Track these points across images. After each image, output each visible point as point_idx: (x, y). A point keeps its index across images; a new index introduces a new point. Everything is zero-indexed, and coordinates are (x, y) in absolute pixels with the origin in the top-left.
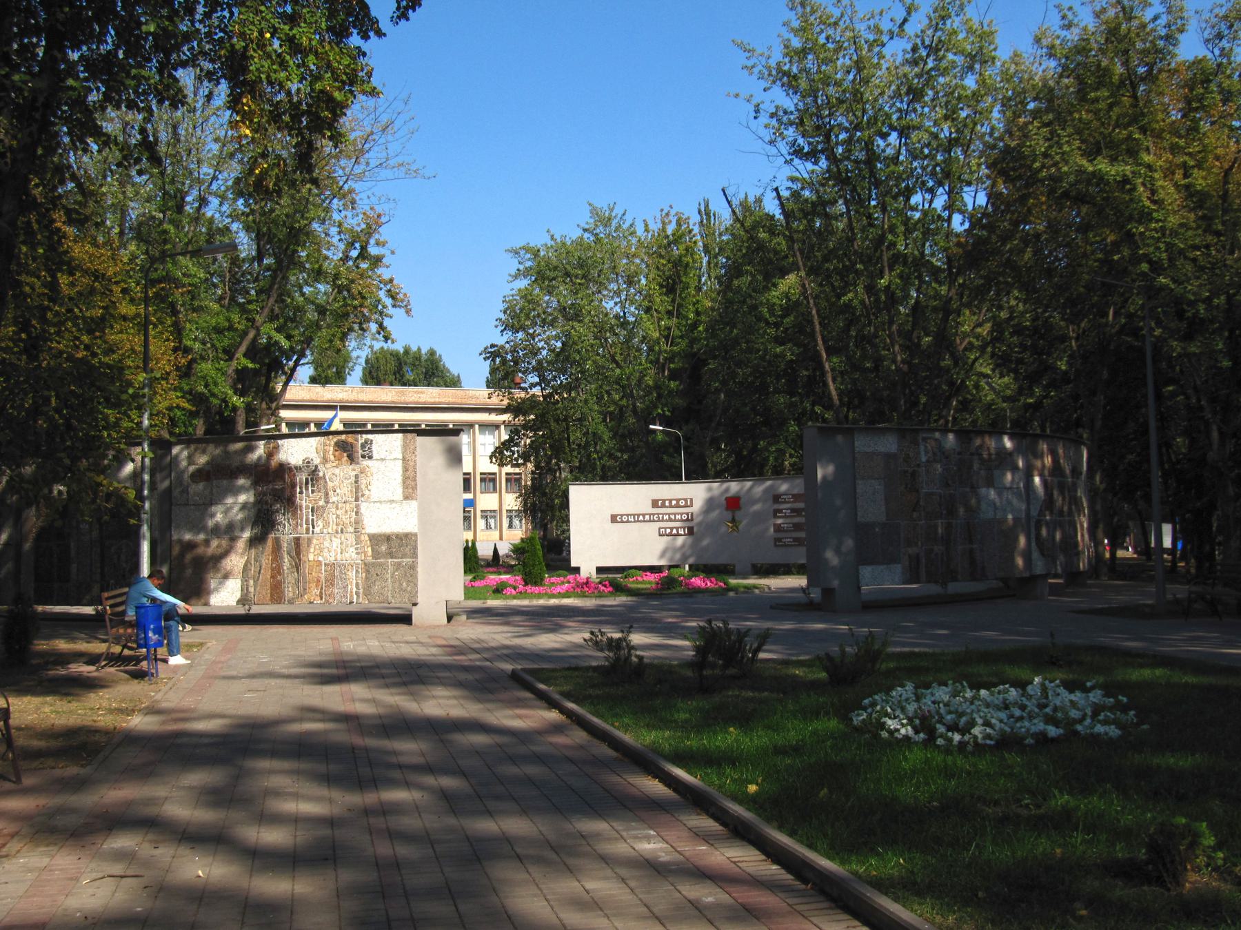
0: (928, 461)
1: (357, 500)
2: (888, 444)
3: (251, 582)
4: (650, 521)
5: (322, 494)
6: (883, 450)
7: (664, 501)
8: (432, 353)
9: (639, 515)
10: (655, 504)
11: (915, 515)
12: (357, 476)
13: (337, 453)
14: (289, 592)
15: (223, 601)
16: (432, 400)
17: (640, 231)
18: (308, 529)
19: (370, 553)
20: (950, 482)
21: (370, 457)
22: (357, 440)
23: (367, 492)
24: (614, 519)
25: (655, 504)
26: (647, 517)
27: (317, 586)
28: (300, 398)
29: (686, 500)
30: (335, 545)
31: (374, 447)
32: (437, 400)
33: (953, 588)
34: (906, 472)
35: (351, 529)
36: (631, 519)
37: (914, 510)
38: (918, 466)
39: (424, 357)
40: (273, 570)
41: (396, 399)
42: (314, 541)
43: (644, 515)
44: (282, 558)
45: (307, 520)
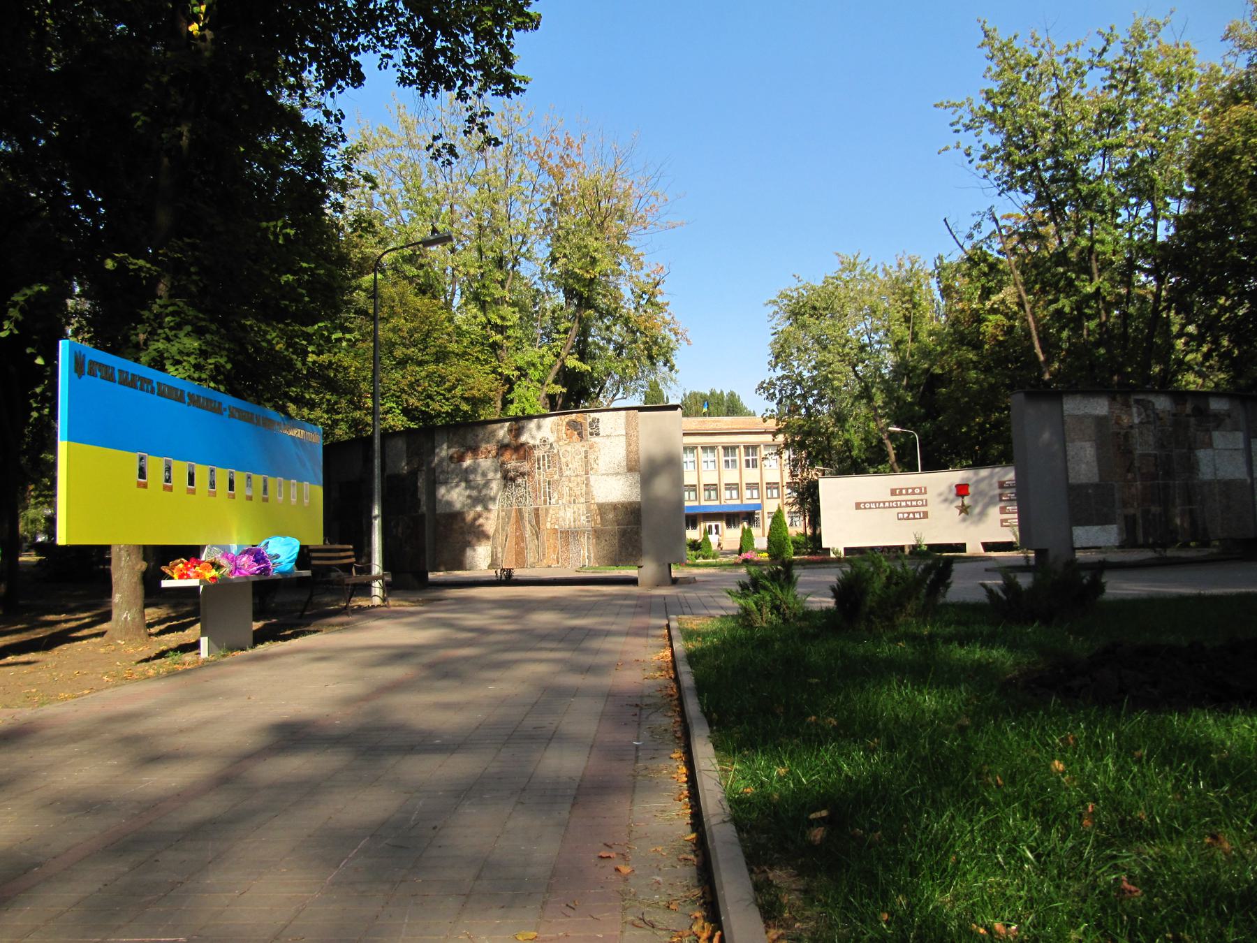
0: (1141, 423)
1: (587, 473)
2: (1100, 407)
3: (499, 549)
4: (889, 507)
5: (557, 469)
7: (901, 490)
8: (732, 395)
9: (879, 503)
10: (893, 492)
11: (1130, 476)
12: (586, 452)
13: (569, 432)
14: (531, 557)
17: (880, 276)
19: (599, 521)
20: (1165, 443)
22: (585, 419)
23: (595, 466)
24: (858, 506)
25: (893, 492)
26: (887, 504)
27: (554, 551)
29: (920, 488)
30: (569, 514)
31: (600, 425)
33: (1171, 553)
35: (583, 500)
36: (873, 506)
37: (1128, 471)
38: (1131, 427)
39: (726, 398)
40: (517, 537)
41: (698, 427)
42: (551, 511)
43: (884, 503)
44: (524, 527)
45: (545, 492)
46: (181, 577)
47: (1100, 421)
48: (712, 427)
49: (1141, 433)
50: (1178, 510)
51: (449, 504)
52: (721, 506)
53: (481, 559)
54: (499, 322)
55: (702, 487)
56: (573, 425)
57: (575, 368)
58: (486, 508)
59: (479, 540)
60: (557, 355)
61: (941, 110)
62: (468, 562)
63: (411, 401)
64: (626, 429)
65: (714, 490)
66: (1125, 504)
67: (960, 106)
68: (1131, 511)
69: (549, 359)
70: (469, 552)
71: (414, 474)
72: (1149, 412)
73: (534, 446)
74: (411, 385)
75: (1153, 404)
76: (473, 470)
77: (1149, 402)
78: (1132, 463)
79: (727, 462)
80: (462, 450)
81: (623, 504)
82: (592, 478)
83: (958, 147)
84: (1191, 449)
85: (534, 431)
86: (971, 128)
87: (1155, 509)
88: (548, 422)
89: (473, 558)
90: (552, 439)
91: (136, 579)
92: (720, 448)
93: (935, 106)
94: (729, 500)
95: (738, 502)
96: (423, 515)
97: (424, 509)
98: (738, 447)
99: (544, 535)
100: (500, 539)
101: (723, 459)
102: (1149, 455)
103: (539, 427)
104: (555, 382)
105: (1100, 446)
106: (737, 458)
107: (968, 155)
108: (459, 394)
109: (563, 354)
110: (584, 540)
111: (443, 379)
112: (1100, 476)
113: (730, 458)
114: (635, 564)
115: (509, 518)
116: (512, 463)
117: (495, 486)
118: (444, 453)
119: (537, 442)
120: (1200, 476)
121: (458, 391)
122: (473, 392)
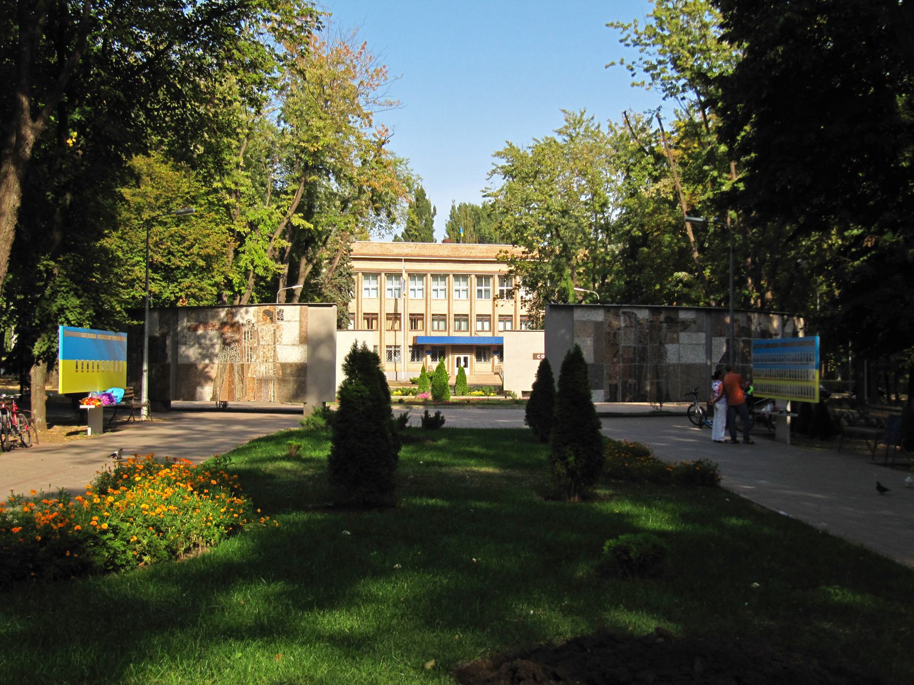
0: (626, 327)
1: (274, 343)
3: (218, 389)
5: (256, 340)
6: (593, 319)
11: (615, 360)
12: (275, 330)
14: (238, 395)
15: (722, 422)
16: (481, 255)
17: (605, 130)
18: (248, 360)
19: (281, 374)
20: (642, 340)
21: (282, 320)
22: (275, 309)
23: (280, 340)
28: (374, 253)
32: (485, 255)
33: (669, 406)
34: (610, 333)
35: (271, 360)
37: (615, 356)
38: (619, 329)
41: (451, 254)
42: (251, 366)
44: (234, 375)
45: (248, 354)
46: (87, 404)
47: (598, 325)
48: (465, 254)
49: (625, 334)
50: (648, 383)
51: (187, 357)
52: (471, 337)
53: (207, 393)
54: (233, 187)
55: (452, 317)
56: (267, 313)
57: (299, 226)
58: (211, 361)
59: (206, 382)
60: (285, 214)
61: (611, 29)
62: (198, 396)
63: (156, 257)
64: (300, 317)
65: (465, 320)
66: (610, 377)
67: (625, 29)
68: (615, 382)
69: (278, 215)
70: (199, 389)
71: (164, 336)
72: (633, 320)
73: (242, 324)
74: (156, 244)
75: (636, 315)
76: (204, 336)
77: (633, 313)
78: (618, 352)
79: (480, 291)
80: (196, 324)
81: (296, 364)
82: (278, 347)
83: (622, 63)
84: (661, 344)
85: (244, 315)
86: (638, 44)
87: (631, 381)
88: (252, 310)
89: (201, 393)
90: (253, 321)
91: (43, 403)
92: (473, 276)
93: (607, 25)
94: (480, 332)
95: (490, 334)
96: (169, 365)
97: (169, 360)
98: (492, 276)
99: (247, 381)
100: (219, 382)
101: (476, 288)
102: (630, 347)
103: (247, 312)
104: (283, 236)
105: (597, 341)
106: (491, 288)
107: (632, 70)
108: (196, 252)
109: (290, 213)
110: (271, 385)
111: (184, 239)
112: (595, 359)
113: (483, 288)
114: (302, 402)
115: (225, 370)
116: (229, 333)
117: (217, 348)
118: (185, 324)
119: (245, 322)
120: (668, 361)
121: (195, 250)
122: (208, 250)
